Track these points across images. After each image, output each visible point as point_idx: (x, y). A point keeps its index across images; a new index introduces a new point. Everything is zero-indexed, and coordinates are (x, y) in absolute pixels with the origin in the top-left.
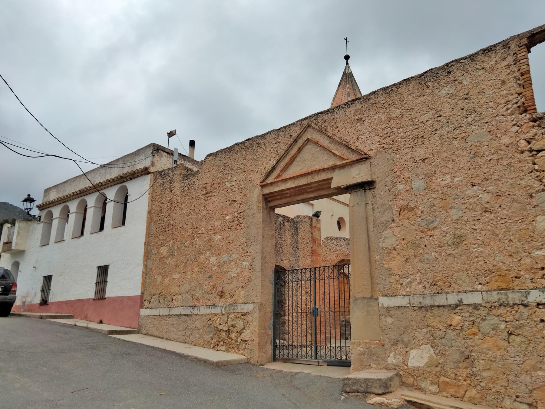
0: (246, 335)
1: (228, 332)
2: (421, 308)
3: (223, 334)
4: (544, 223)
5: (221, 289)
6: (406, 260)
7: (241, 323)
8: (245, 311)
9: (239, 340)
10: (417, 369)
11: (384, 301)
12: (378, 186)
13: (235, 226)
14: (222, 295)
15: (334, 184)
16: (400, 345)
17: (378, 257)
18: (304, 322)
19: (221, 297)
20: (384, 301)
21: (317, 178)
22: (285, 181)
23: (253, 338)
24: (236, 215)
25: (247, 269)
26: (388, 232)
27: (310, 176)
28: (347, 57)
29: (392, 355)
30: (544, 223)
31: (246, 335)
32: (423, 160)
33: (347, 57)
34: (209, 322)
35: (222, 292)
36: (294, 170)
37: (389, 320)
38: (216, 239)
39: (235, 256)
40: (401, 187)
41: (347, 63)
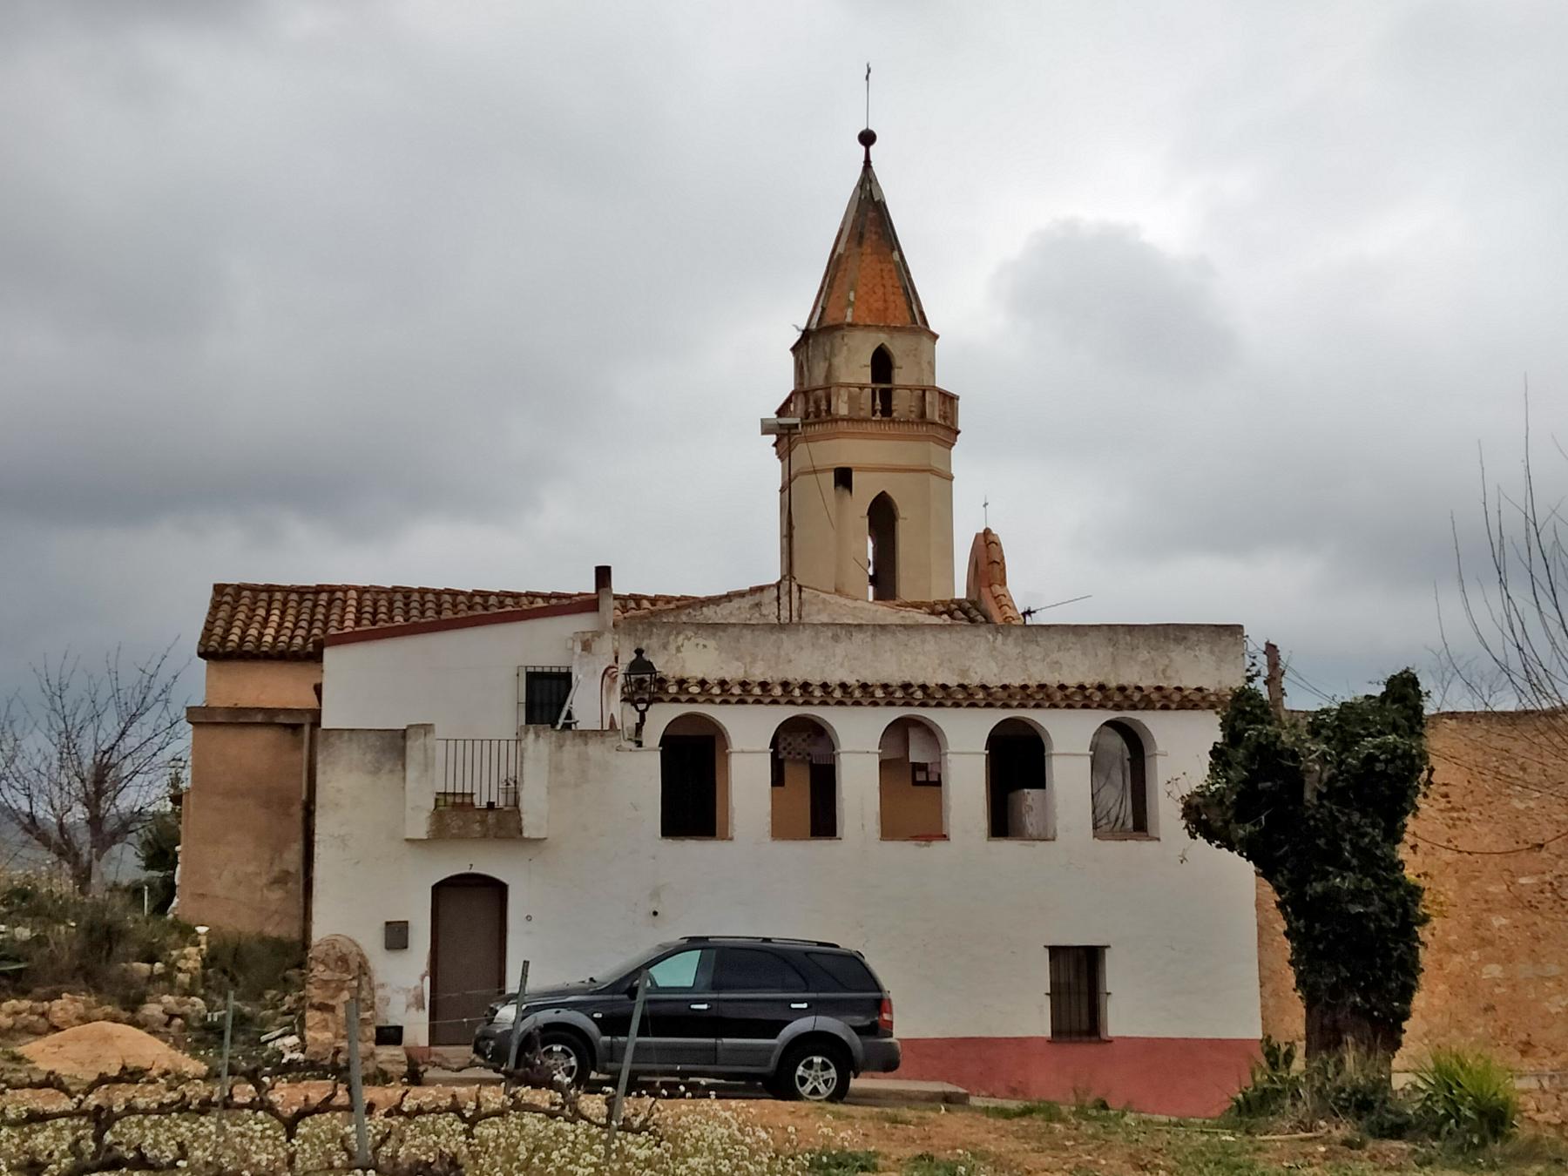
5: (1524, 1037)
14: (1526, 1048)
24: (1548, 878)
28: (867, 138)
33: (867, 138)
39: (1553, 969)
41: (867, 162)
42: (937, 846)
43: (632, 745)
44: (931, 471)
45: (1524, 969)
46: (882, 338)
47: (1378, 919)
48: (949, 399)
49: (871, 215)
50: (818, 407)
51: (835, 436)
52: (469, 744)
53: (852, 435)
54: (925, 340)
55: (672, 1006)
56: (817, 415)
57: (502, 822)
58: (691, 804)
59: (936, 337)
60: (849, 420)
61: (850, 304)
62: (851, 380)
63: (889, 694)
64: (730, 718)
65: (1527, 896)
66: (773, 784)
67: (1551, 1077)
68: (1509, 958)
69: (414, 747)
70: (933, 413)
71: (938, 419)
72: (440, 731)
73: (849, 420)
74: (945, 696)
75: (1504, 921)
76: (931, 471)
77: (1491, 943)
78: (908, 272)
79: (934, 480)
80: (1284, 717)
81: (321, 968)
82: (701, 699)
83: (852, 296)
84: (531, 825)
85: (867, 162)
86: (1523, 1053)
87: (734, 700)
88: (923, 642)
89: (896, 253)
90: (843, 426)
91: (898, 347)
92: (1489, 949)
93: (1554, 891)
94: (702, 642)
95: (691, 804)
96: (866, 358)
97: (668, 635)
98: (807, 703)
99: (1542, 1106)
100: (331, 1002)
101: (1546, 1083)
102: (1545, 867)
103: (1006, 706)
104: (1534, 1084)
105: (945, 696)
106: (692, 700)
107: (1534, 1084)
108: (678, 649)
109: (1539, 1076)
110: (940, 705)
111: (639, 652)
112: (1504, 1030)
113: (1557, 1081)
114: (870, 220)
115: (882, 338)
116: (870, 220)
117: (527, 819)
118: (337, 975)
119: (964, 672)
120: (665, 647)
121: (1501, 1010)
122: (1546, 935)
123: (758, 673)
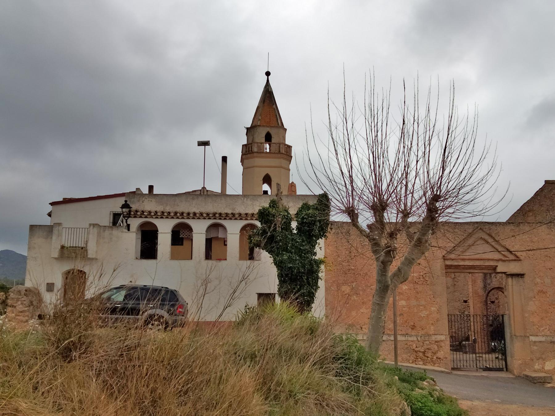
0: (441, 354)
1: (424, 353)
2: (551, 342)
3: (421, 354)
4: (0, 322)
5: (412, 324)
6: (542, 319)
7: (436, 347)
8: (438, 339)
9: (435, 357)
10: (549, 370)
11: (533, 338)
12: (526, 276)
13: (421, 283)
14: (413, 327)
15: (499, 270)
16: (541, 360)
17: (526, 315)
18: (483, 346)
19: (412, 329)
20: (533, 338)
21: (487, 263)
22: (463, 260)
23: (447, 356)
24: (422, 274)
25: (436, 313)
26: (531, 303)
27: (482, 261)
28: (268, 74)
29: (537, 364)
30: (0, 322)
31: (441, 354)
32: (550, 269)
33: (268, 74)
34: (406, 346)
35: (414, 326)
36: (467, 254)
37: (535, 348)
38: (404, 288)
39: (423, 303)
40: (538, 280)
41: (268, 80)
42: (223, 262)
43: (127, 231)
44: (282, 167)
45: (414, 302)
46: (268, 129)
47: (298, 269)
48: (290, 147)
49: (268, 95)
50: (249, 149)
51: (254, 157)
52: (75, 229)
53: (260, 157)
54: (281, 131)
55: (418, 370)
56: (249, 151)
57: (80, 252)
58: (148, 250)
59: (286, 130)
60: (257, 152)
61: (259, 120)
62: (259, 141)
63: (208, 216)
64: (158, 223)
65: (415, 279)
66: (172, 245)
67: (421, 337)
68: (408, 299)
69: (55, 231)
70: (283, 151)
71: (286, 153)
72: (64, 226)
73: (257, 152)
74: (227, 216)
75: (406, 287)
76: (282, 167)
77: (402, 294)
78: (278, 111)
79: (283, 170)
80: (281, 206)
81: (12, 294)
82: (154, 217)
83: (260, 118)
84: (91, 254)
85: (268, 80)
86: (412, 329)
87: (159, 217)
88: (221, 200)
89: (274, 106)
90: (255, 154)
91: (273, 132)
92: (401, 296)
93: (423, 278)
94: (150, 200)
95: (148, 250)
96: (264, 135)
97: (140, 198)
98: (183, 218)
99: (418, 346)
100: (15, 305)
101: (419, 339)
102: (420, 271)
103: (246, 219)
104: (415, 339)
105: (227, 216)
106: (146, 217)
107: (415, 339)
108: (143, 202)
109: (417, 336)
110: (225, 219)
111: (126, 201)
112: (406, 322)
113: (423, 338)
114: (268, 96)
115: (268, 129)
116: (268, 96)
117: (90, 252)
118: (17, 297)
119: (234, 209)
120: (139, 201)
121: (405, 315)
122: (421, 292)
123: (168, 209)
